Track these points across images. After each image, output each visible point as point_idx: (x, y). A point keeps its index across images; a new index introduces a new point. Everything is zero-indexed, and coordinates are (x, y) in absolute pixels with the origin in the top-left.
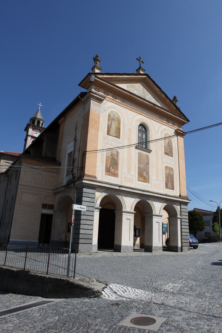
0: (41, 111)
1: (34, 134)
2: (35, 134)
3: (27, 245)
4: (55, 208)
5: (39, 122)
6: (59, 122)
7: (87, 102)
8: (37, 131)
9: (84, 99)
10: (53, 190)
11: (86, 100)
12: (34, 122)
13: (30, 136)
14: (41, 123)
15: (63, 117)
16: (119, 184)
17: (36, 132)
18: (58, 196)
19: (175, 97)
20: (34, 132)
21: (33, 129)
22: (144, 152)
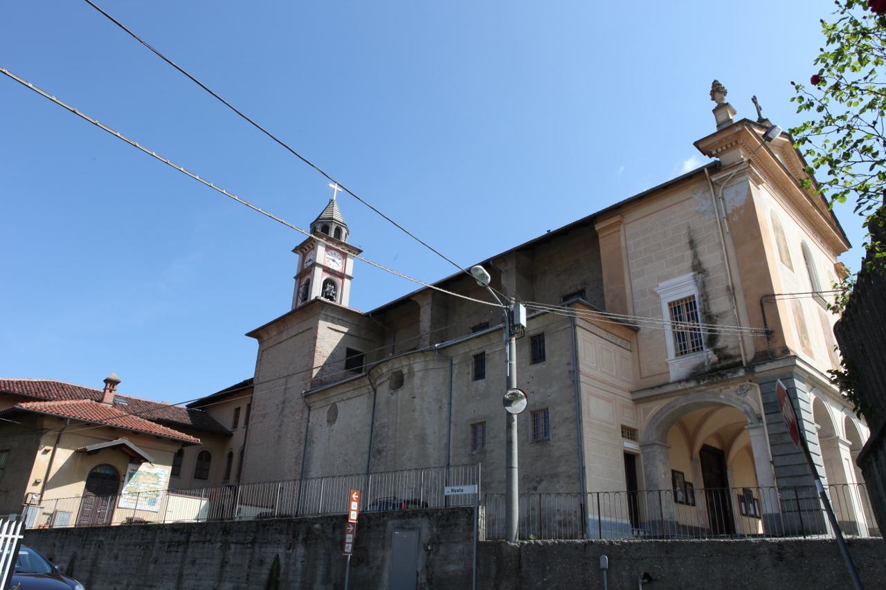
0: (339, 205)
1: (328, 261)
2: (331, 262)
3: (598, 493)
4: (640, 436)
5: (338, 231)
6: (598, 227)
7: (730, 185)
8: (335, 254)
9: (729, 173)
10: (632, 392)
11: (733, 177)
12: (326, 229)
13: (320, 265)
14: (344, 235)
15: (619, 216)
16: (152, 520)
17: (333, 258)
18: (656, 407)
19: (864, 227)
20: (328, 256)
21: (328, 248)
22: (141, 454)
